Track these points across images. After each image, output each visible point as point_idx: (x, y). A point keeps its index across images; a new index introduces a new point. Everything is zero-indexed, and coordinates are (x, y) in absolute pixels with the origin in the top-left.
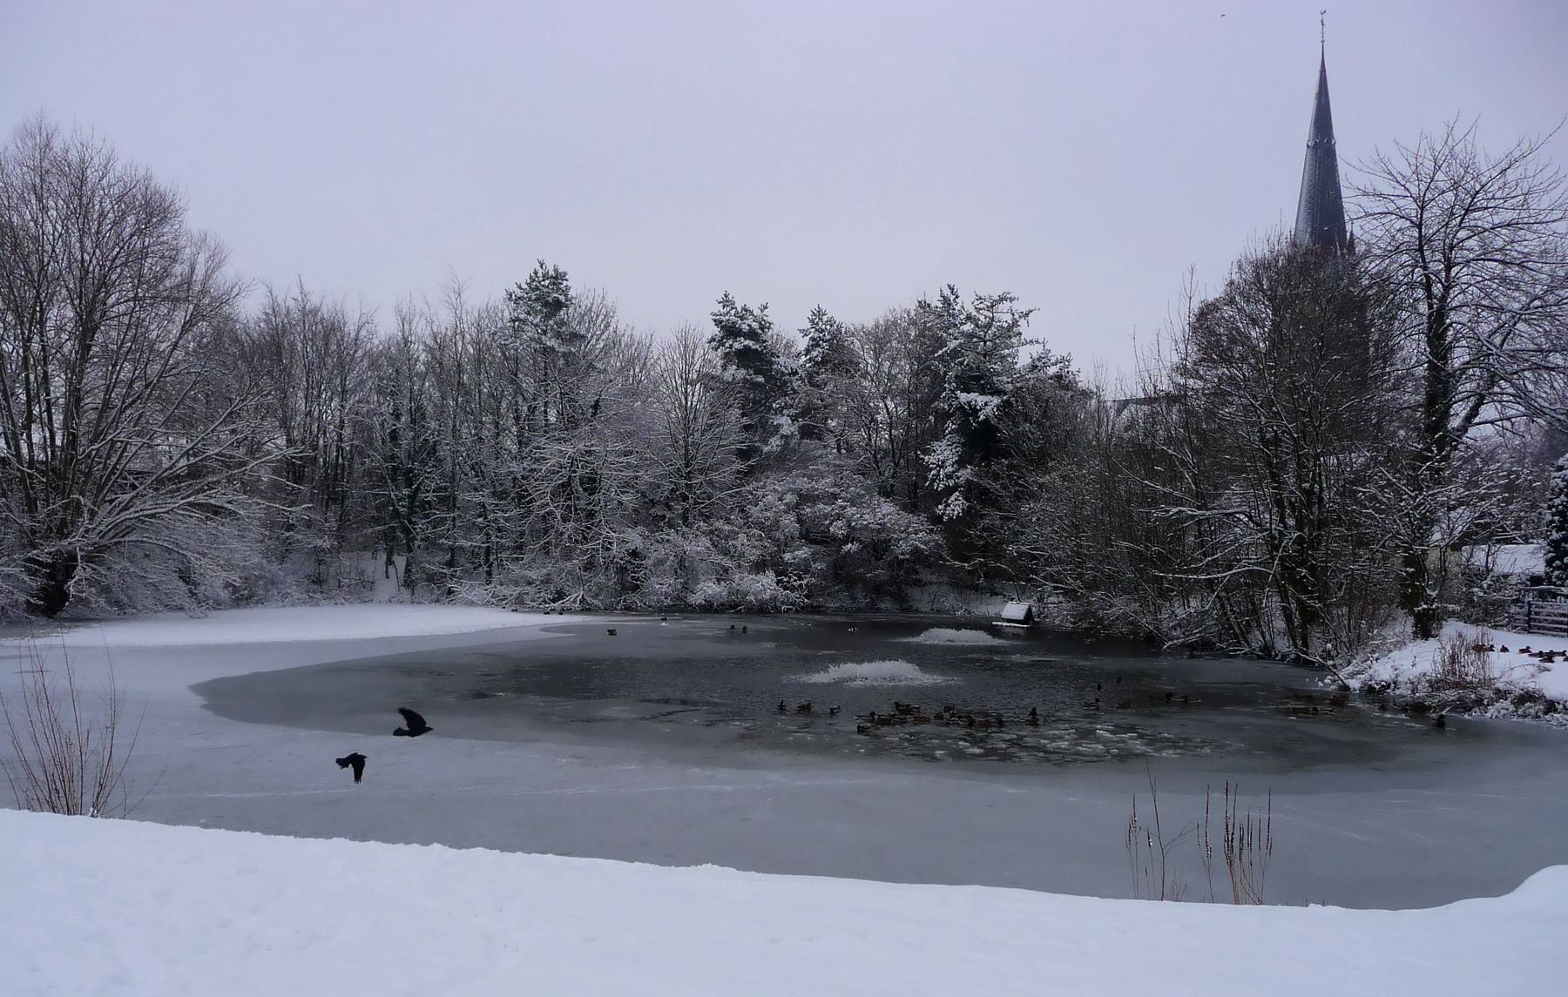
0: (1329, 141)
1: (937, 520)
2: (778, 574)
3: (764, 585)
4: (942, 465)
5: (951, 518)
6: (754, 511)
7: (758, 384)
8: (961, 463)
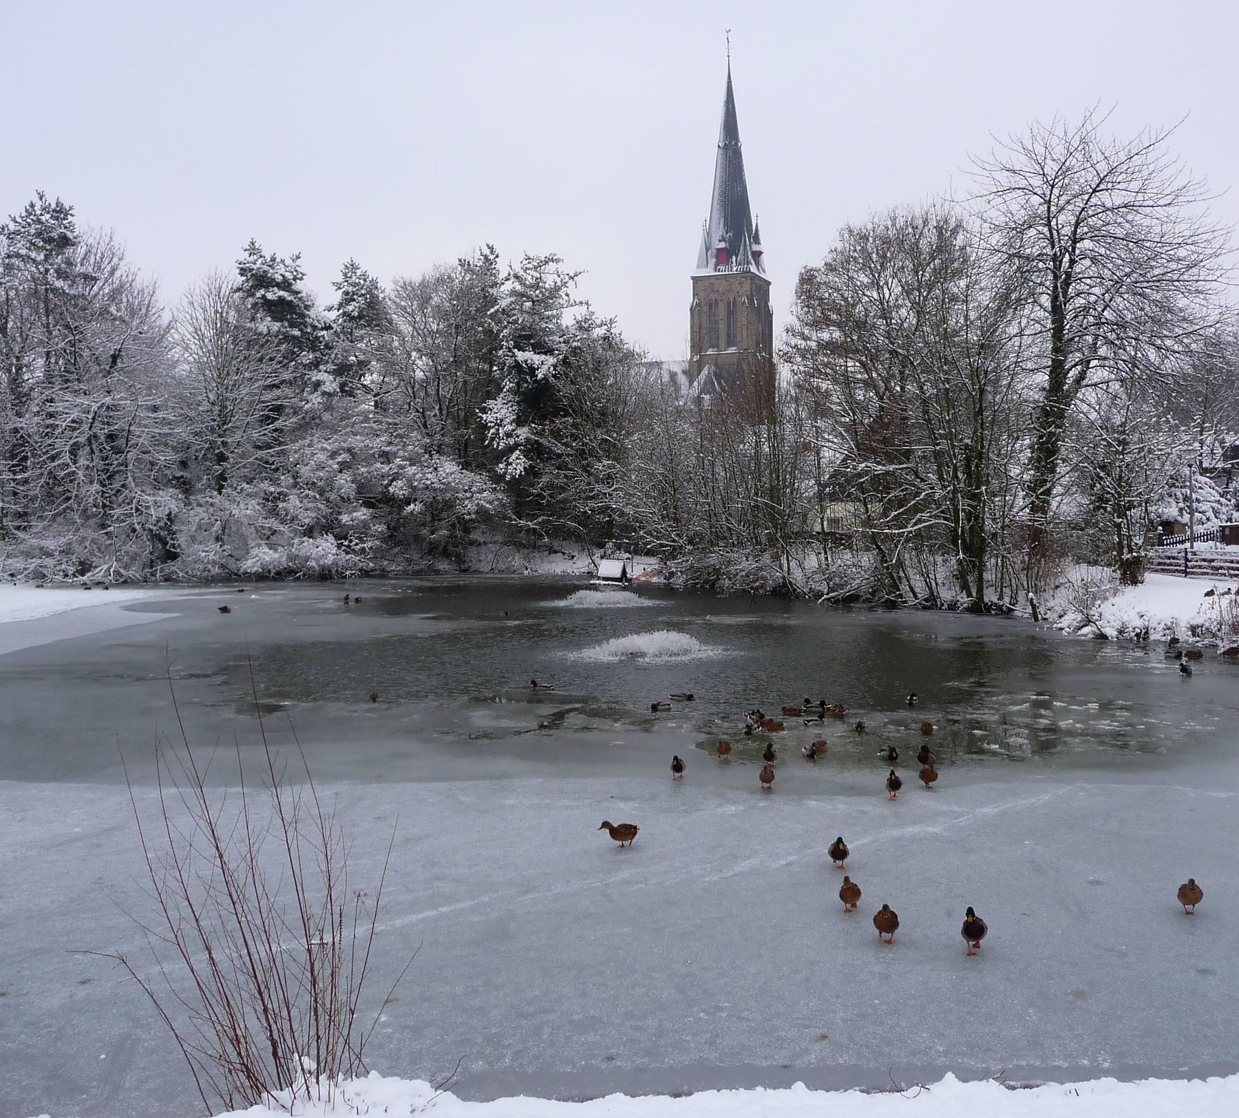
0: (736, 144)
1: (498, 479)
2: (337, 537)
3: (324, 550)
4: (500, 424)
5: (513, 477)
6: (304, 471)
7: (294, 337)
8: (519, 422)
